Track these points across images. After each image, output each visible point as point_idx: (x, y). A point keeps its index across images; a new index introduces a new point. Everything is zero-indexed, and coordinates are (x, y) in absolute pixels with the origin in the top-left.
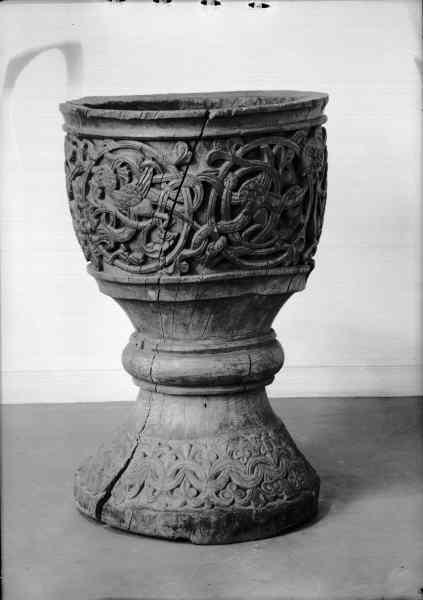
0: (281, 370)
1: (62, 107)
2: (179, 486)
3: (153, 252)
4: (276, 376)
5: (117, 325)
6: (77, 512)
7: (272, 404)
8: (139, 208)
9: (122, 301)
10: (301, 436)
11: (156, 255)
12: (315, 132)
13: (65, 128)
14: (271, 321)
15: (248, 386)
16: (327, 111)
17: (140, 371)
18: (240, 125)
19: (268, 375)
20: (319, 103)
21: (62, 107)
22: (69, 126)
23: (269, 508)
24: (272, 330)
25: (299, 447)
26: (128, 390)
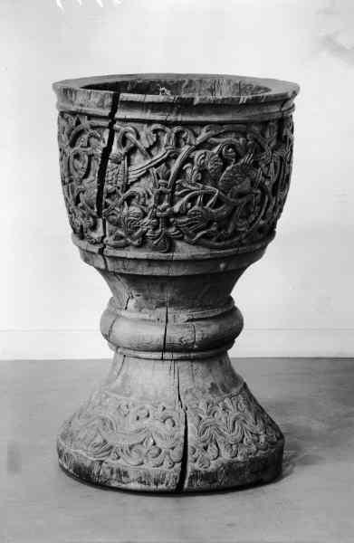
0: (242, 334)
1: (55, 86)
2: (244, 436)
3: (241, 227)
4: (236, 340)
5: (95, 290)
6: (58, 467)
7: (232, 364)
8: (242, 187)
9: (104, 272)
10: (263, 392)
11: (243, 229)
12: (283, 126)
13: (58, 106)
14: (230, 291)
15: (213, 350)
16: (296, 101)
17: (144, 339)
18: (218, 113)
19: (227, 339)
20: (284, 100)
21: (55, 86)
22: (61, 104)
23: (76, 453)
24: (231, 299)
25: (260, 402)
26: (107, 353)
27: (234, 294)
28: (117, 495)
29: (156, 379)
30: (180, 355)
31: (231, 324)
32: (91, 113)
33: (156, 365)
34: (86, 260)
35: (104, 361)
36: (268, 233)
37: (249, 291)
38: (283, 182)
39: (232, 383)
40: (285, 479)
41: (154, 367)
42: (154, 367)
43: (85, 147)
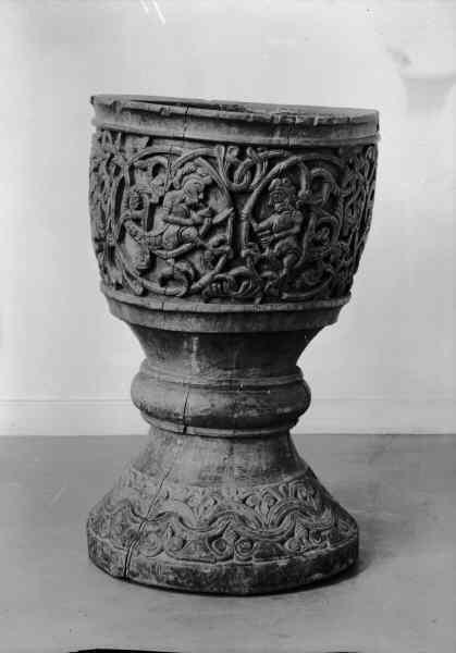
12: (368, 150)
14: (299, 353)
26: (141, 426)
27: (300, 363)
28: (138, 587)
29: (199, 455)
30: (229, 433)
31: (300, 398)
32: (152, 134)
33: (235, 446)
34: (114, 313)
35: (135, 438)
36: (342, 291)
37: (318, 360)
38: (364, 225)
39: (285, 459)
40: (361, 574)
41: (232, 449)
42: (232, 449)
43: (341, 232)
